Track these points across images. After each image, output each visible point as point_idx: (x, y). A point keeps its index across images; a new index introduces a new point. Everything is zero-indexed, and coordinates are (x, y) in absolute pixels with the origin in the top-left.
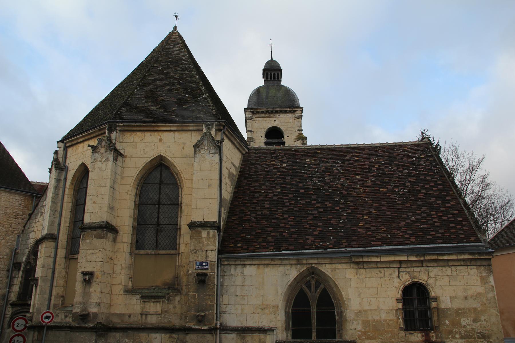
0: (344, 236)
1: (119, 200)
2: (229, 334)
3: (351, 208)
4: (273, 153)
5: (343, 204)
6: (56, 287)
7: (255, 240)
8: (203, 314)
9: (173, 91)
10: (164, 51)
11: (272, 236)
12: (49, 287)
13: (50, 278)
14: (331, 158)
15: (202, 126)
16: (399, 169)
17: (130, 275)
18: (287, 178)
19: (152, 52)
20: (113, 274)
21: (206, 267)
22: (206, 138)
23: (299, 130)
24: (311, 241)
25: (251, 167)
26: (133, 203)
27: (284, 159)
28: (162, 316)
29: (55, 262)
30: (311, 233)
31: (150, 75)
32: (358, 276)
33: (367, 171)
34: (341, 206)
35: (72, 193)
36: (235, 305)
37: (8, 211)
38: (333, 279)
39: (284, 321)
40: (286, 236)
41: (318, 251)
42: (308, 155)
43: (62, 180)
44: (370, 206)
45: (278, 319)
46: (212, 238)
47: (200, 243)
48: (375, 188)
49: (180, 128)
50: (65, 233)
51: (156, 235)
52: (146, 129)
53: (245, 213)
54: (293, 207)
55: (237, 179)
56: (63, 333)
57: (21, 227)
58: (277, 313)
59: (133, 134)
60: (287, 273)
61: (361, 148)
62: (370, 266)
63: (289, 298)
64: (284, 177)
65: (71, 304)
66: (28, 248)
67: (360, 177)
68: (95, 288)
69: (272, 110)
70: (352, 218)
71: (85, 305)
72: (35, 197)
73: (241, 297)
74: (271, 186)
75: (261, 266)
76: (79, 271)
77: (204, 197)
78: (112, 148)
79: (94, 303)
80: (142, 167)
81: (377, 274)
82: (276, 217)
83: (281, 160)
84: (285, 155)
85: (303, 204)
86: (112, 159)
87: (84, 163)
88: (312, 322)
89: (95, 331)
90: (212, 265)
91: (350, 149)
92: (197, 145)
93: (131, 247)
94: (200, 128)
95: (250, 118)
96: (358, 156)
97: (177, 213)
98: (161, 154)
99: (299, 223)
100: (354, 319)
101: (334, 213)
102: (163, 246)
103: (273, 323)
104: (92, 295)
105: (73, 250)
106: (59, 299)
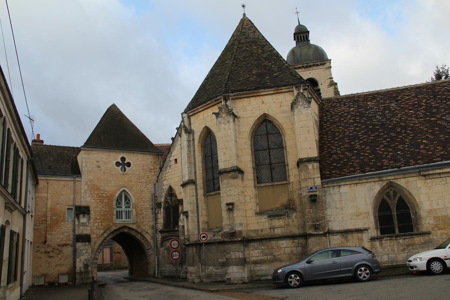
0: (411, 156)
2: (335, 236)
3: (411, 135)
4: (341, 101)
5: (404, 133)
6: (201, 216)
7: (344, 167)
8: (318, 223)
9: (261, 64)
10: (243, 35)
11: (357, 163)
12: (197, 217)
13: (196, 211)
14: (386, 99)
15: (293, 88)
16: (443, 102)
18: (356, 119)
21: (315, 190)
23: (330, 78)
24: (386, 163)
25: (327, 113)
28: (285, 228)
29: (197, 199)
30: (385, 157)
31: (239, 54)
32: (426, 185)
33: (417, 106)
34: (403, 135)
36: (336, 215)
37: (144, 168)
38: (407, 189)
41: (393, 170)
42: (368, 99)
44: (425, 132)
45: (370, 222)
47: (308, 173)
48: (427, 119)
49: (276, 92)
52: (251, 95)
54: (366, 140)
56: (214, 247)
57: (155, 178)
60: (372, 187)
61: (408, 89)
62: (435, 176)
64: (354, 118)
67: (413, 111)
68: (236, 213)
69: (306, 65)
70: (414, 143)
72: (160, 155)
73: (340, 209)
78: (231, 113)
79: (238, 224)
80: (253, 124)
81: (441, 182)
83: (348, 105)
84: (350, 101)
85: (373, 136)
88: (394, 221)
89: (242, 242)
91: (400, 91)
93: (254, 183)
94: (291, 90)
96: (407, 96)
97: (283, 154)
98: (265, 112)
99: (374, 151)
100: (427, 216)
101: (399, 141)
102: (277, 179)
103: (366, 225)
104: (236, 218)
105: (208, 189)
106: (205, 225)
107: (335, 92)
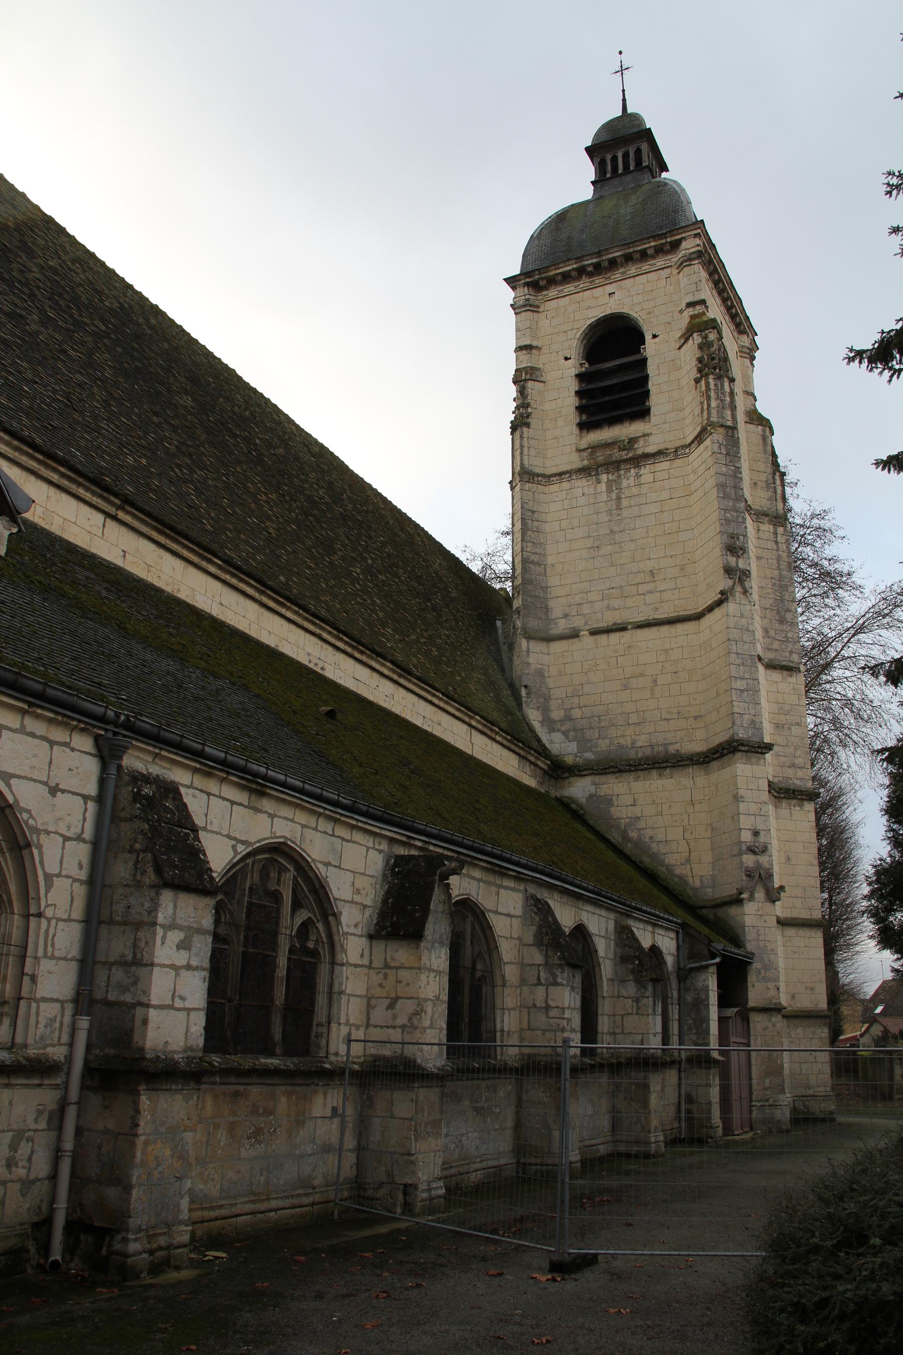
69: (594, 261)
95: (524, 306)
107: (700, 360)
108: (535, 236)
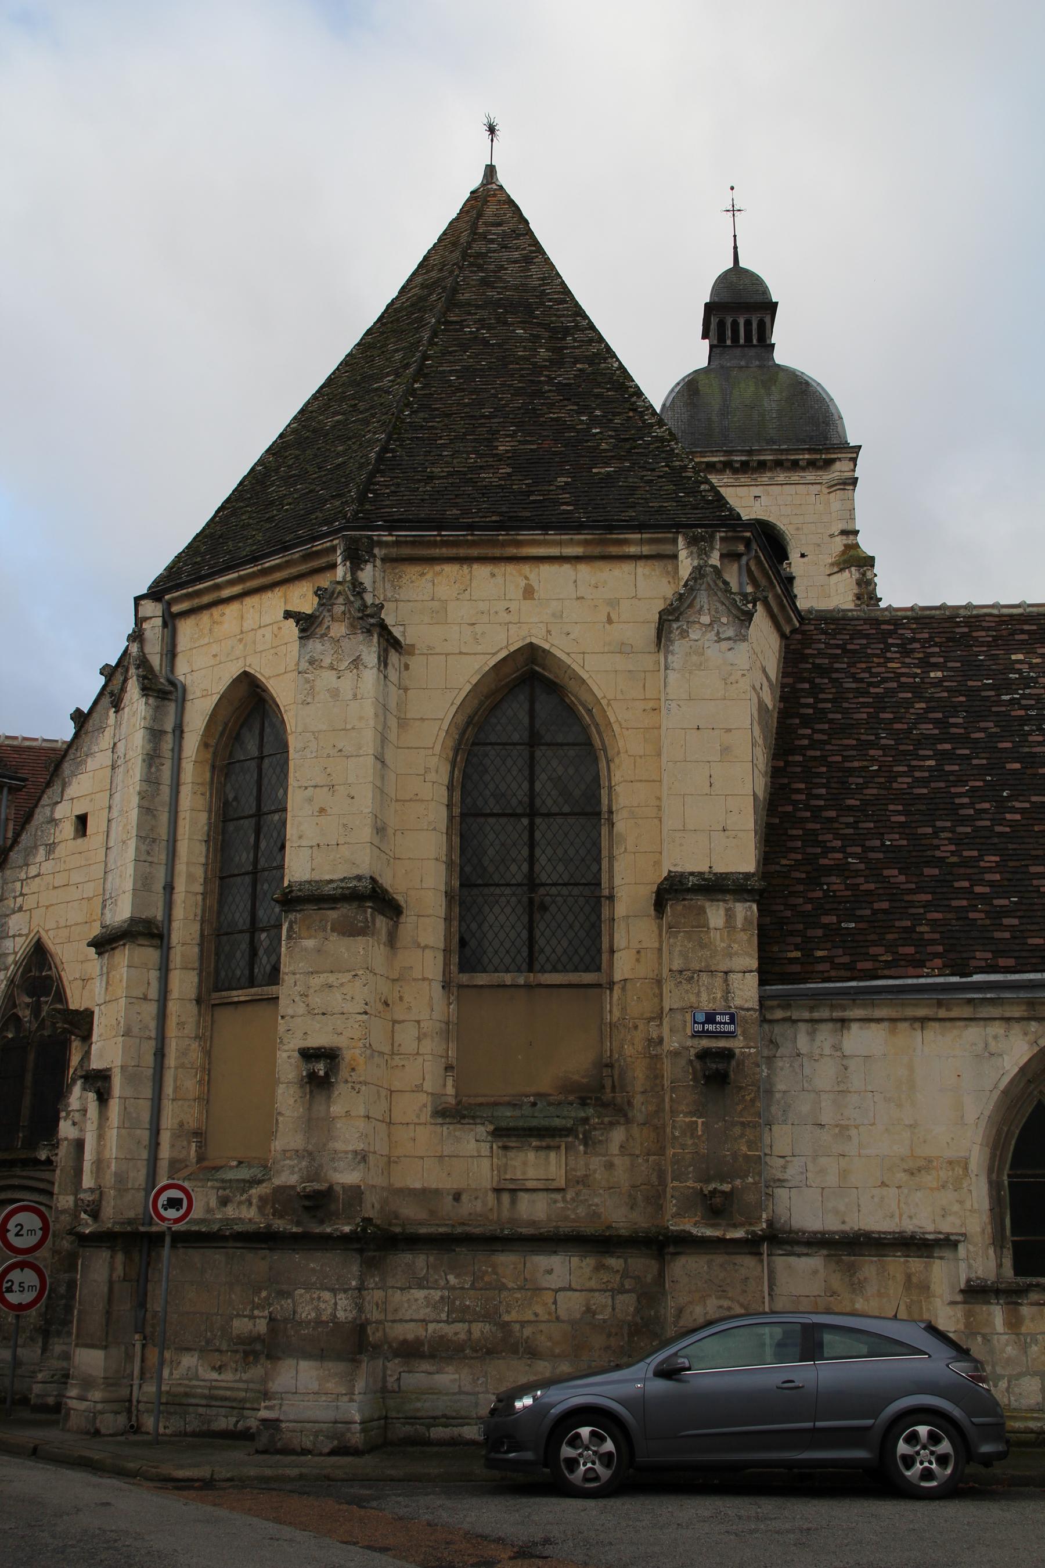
1: (397, 801)
2: (799, 1255)
4: (890, 633)
6: (173, 1100)
8: (726, 1187)
10: (471, 265)
12: (149, 1103)
13: (150, 1072)
15: (675, 541)
17: (447, 1057)
19: (421, 265)
20: (393, 1054)
22: (704, 587)
23: (844, 533)
25: (817, 681)
26: (444, 812)
27: (933, 655)
28: (569, 1197)
29: (162, 1016)
31: (444, 354)
35: (208, 775)
36: (815, 1157)
39: (988, 1213)
40: (979, 922)
42: (1017, 637)
43: (166, 732)
45: (968, 1205)
46: (743, 930)
47: (702, 946)
49: (597, 551)
50: (192, 917)
51: (525, 919)
52: (475, 552)
53: (825, 842)
54: (988, 823)
55: (775, 725)
56: (218, 1257)
58: (965, 1185)
59: (431, 571)
63: (999, 1132)
64: (940, 715)
65: (233, 1159)
66: (7, 969)
69: (744, 458)
71: (314, 1160)
72: (5, 790)
73: (837, 1130)
74: (902, 747)
75: (903, 1026)
76: (286, 1048)
77: (707, 790)
78: (372, 621)
79: (346, 1152)
80: (468, 687)
82: (933, 856)
83: (921, 655)
84: (931, 638)
85: (1022, 811)
86: (376, 660)
87: (252, 672)
90: (746, 1022)
92: (675, 610)
93: (446, 964)
94: (667, 549)
98: (535, 641)
103: (950, 1219)
105: (223, 974)
106: (185, 1143)
108: (668, 404)
